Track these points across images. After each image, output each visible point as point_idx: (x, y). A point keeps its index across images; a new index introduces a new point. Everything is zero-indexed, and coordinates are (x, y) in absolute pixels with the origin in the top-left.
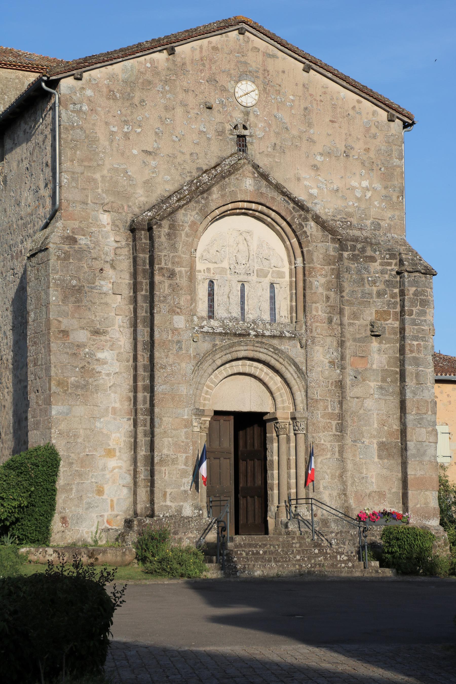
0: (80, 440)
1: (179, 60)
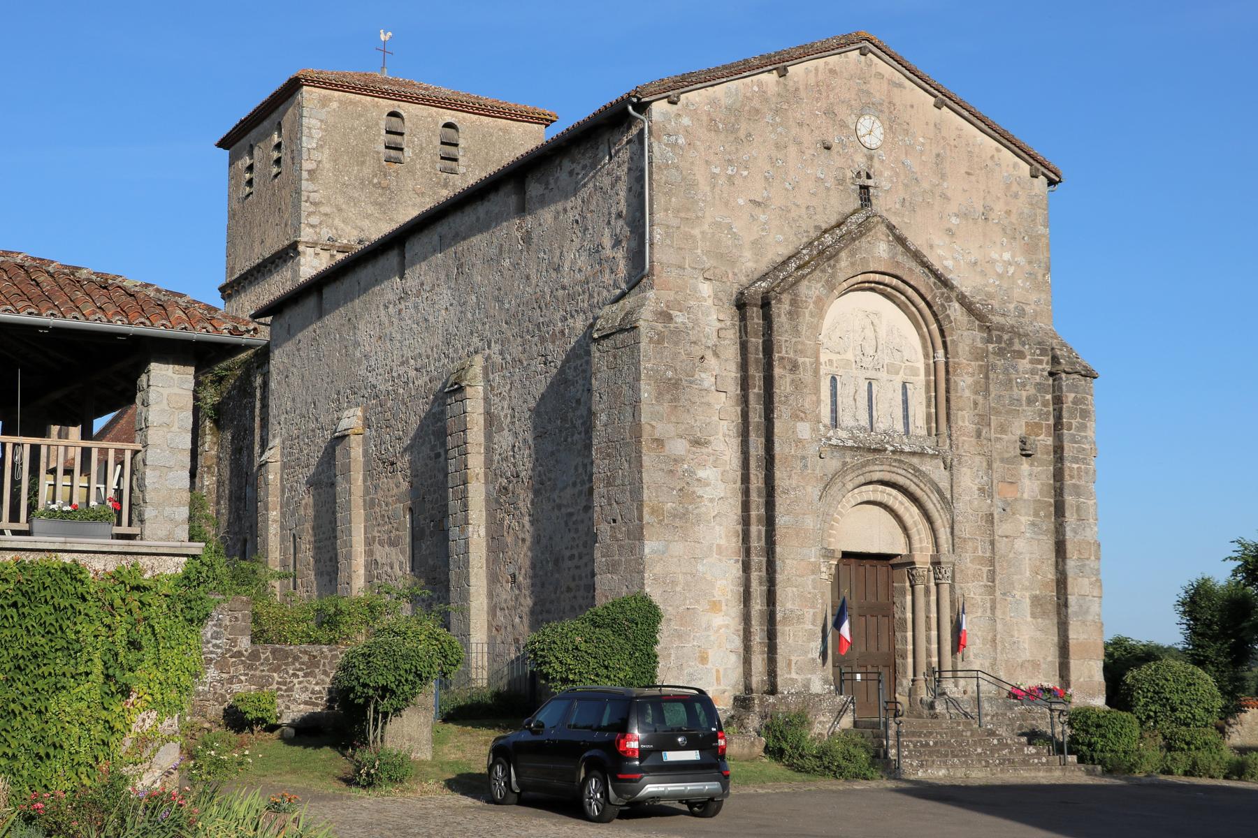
0: (678, 589)
1: (791, 83)
